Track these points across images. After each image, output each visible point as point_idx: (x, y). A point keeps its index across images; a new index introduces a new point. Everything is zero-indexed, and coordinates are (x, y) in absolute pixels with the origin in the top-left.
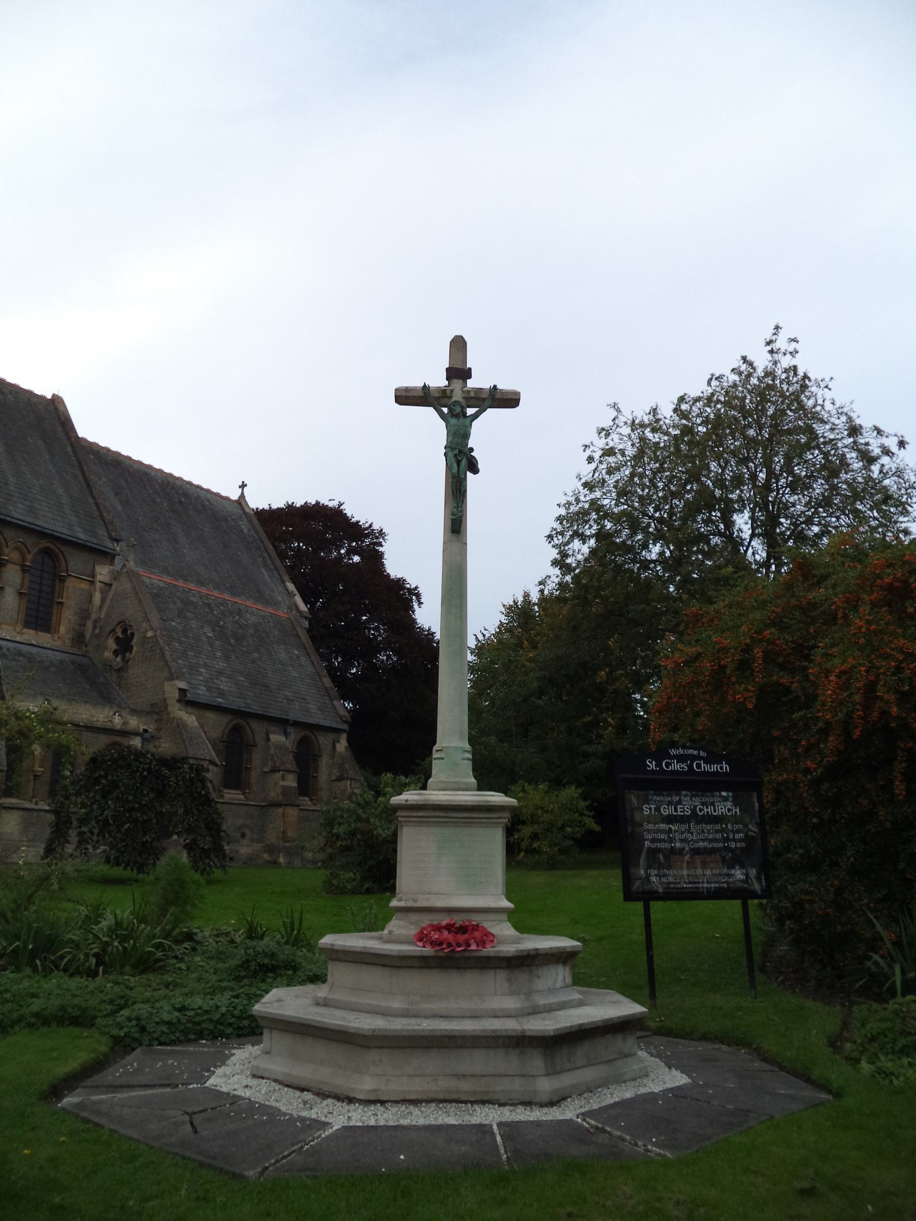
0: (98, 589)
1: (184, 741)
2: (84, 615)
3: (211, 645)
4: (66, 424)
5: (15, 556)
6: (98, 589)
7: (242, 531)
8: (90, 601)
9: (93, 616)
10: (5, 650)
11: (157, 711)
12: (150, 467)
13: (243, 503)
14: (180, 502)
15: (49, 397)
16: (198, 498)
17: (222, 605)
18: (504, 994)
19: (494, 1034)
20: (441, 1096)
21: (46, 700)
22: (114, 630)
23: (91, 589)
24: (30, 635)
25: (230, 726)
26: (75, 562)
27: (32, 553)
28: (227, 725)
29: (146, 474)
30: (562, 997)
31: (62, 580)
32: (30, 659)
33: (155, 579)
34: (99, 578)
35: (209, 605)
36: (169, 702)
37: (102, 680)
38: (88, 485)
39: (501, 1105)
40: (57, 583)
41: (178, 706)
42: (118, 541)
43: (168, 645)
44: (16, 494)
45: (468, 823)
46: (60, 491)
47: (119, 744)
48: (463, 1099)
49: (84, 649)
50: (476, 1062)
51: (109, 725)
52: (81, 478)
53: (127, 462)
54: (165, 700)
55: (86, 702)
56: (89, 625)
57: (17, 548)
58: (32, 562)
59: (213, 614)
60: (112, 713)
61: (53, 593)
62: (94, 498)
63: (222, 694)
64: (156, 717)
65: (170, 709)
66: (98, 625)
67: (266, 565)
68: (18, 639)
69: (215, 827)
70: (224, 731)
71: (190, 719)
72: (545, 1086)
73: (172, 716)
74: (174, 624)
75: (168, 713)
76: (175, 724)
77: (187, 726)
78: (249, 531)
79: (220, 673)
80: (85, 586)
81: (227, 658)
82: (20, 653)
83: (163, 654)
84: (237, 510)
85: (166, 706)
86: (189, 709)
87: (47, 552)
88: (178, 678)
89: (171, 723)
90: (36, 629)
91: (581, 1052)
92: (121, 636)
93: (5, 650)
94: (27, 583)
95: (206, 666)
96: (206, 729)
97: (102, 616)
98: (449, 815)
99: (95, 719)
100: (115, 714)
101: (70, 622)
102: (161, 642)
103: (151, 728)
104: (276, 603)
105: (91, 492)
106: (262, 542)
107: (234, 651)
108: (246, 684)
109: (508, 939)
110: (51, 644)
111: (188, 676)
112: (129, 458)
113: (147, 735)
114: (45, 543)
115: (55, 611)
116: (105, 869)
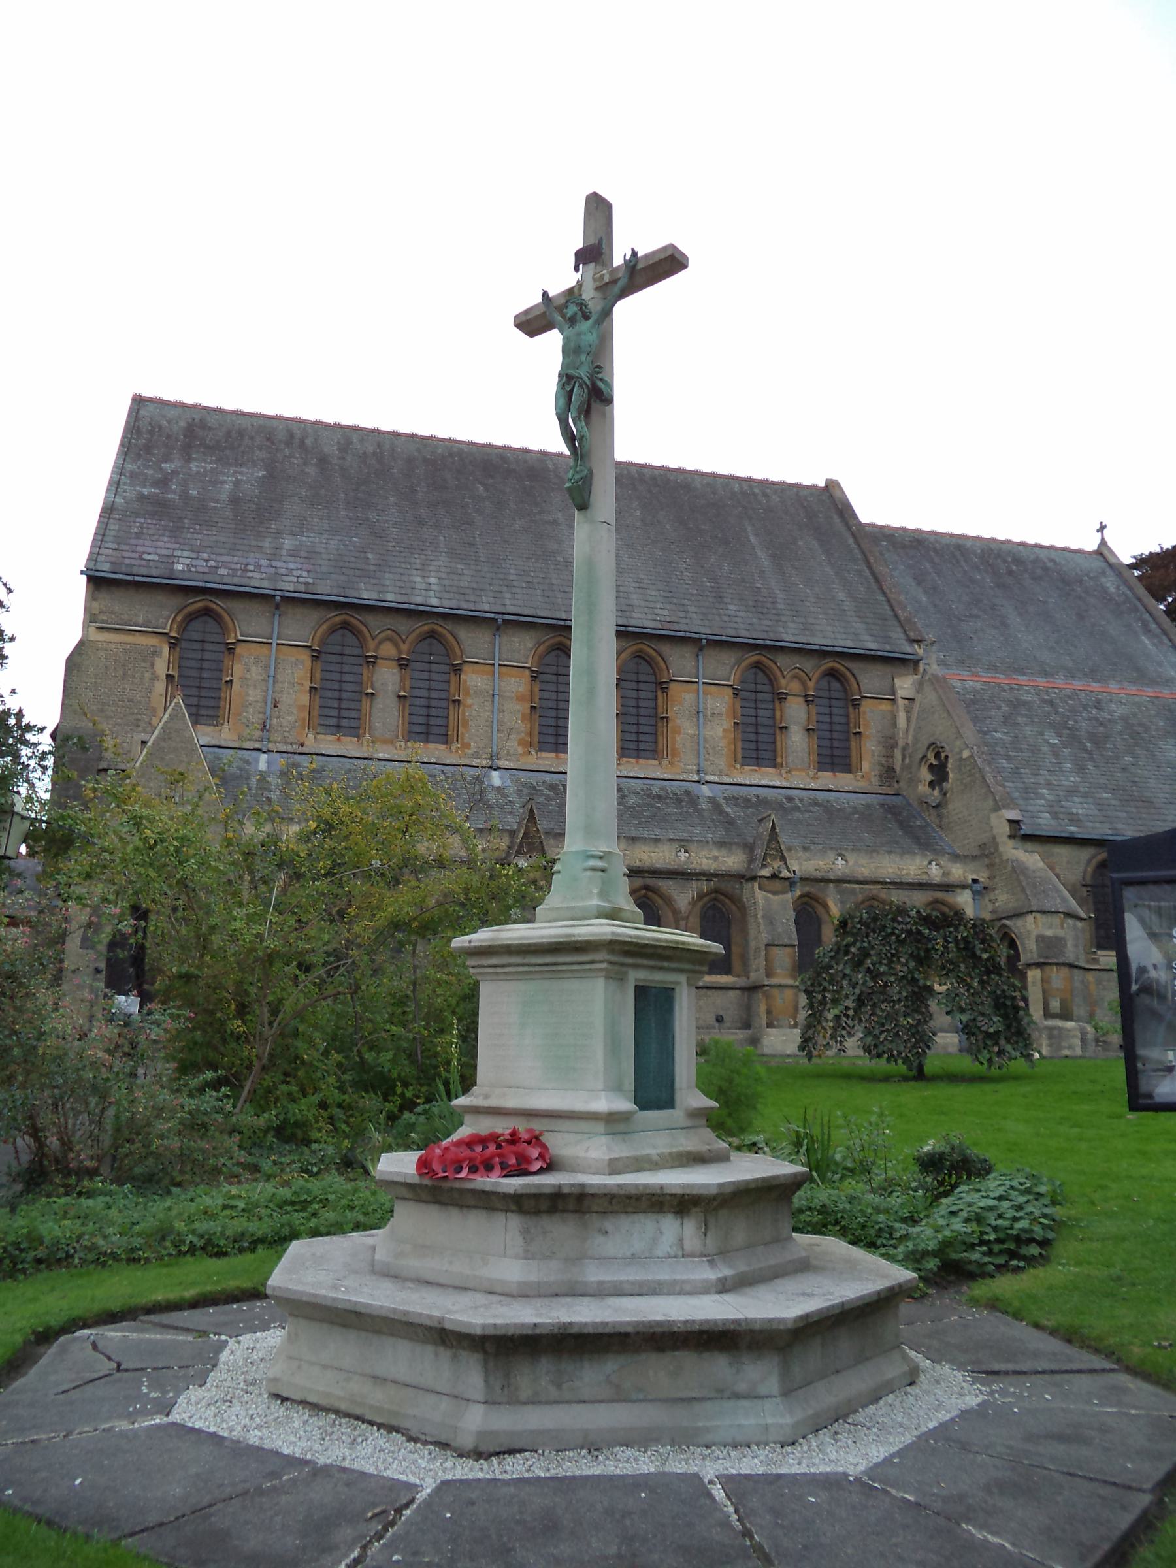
0: (901, 708)
1: (1023, 890)
2: (889, 744)
3: (1056, 755)
4: (844, 510)
5: (795, 686)
6: (901, 708)
7: (1105, 590)
8: (895, 725)
9: (901, 743)
10: (797, 801)
11: (986, 853)
12: (965, 537)
13: (1106, 552)
14: (1010, 573)
15: (822, 484)
16: (1037, 560)
17: (1070, 698)
18: (516, 1257)
19: (404, 1319)
20: (343, 1406)
21: (840, 855)
22: (924, 756)
23: (896, 711)
24: (827, 779)
25: (1094, 862)
26: (869, 679)
27: (814, 680)
28: (1089, 861)
29: (959, 547)
30: (662, 1274)
31: (856, 704)
32: (828, 809)
33: (964, 680)
34: (901, 693)
35: (1051, 703)
36: (999, 840)
37: (918, 823)
38: (877, 580)
39: (411, 1439)
40: (851, 709)
41: (1011, 843)
42: (918, 642)
43: (990, 763)
44: (787, 613)
45: (554, 972)
46: (841, 595)
47: (944, 903)
48: (368, 1417)
49: (896, 785)
50: (402, 1360)
51: (924, 879)
52: (867, 573)
53: (932, 538)
54: (994, 838)
55: (890, 852)
56: (898, 753)
57: (795, 677)
58: (816, 689)
59: (1057, 712)
60: (925, 863)
61: (848, 724)
62: (884, 594)
63: (1074, 819)
64: (987, 861)
65: (1001, 849)
66: (907, 753)
67: (1147, 631)
68: (813, 785)
69: (1009, 1003)
70: (1085, 872)
71: (1031, 859)
72: (475, 1421)
73: (1005, 858)
74: (998, 735)
75: (1000, 855)
76: (1010, 868)
77: (1027, 868)
78: (1118, 588)
79: (1072, 791)
80: (885, 706)
81: (1081, 769)
82: (815, 803)
83: (983, 778)
84: (1098, 564)
85: (996, 845)
86: (1029, 846)
87: (832, 674)
88: (1006, 807)
89: (1005, 868)
90: (832, 771)
91: (592, 1375)
92: (935, 763)
93: (797, 801)
94: (814, 717)
95: (1049, 785)
96: (1058, 870)
97: (910, 742)
98: (526, 961)
99: (904, 872)
100: (930, 863)
101: (873, 755)
102: (979, 761)
103: (983, 876)
104: (1167, 681)
105: (881, 588)
106: (1139, 600)
107: (1092, 759)
108: (1113, 802)
109: (588, 1161)
110: (855, 785)
111: (1021, 802)
112: (935, 533)
113: (977, 887)
114: (828, 664)
115: (853, 744)
116: (866, 1063)
